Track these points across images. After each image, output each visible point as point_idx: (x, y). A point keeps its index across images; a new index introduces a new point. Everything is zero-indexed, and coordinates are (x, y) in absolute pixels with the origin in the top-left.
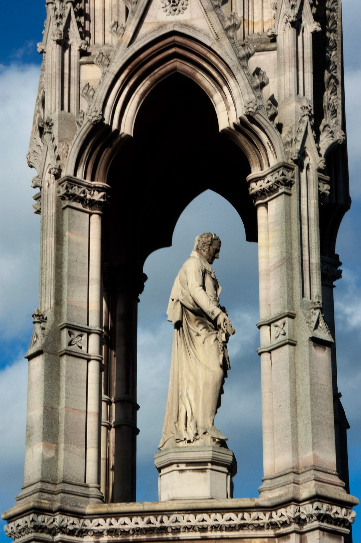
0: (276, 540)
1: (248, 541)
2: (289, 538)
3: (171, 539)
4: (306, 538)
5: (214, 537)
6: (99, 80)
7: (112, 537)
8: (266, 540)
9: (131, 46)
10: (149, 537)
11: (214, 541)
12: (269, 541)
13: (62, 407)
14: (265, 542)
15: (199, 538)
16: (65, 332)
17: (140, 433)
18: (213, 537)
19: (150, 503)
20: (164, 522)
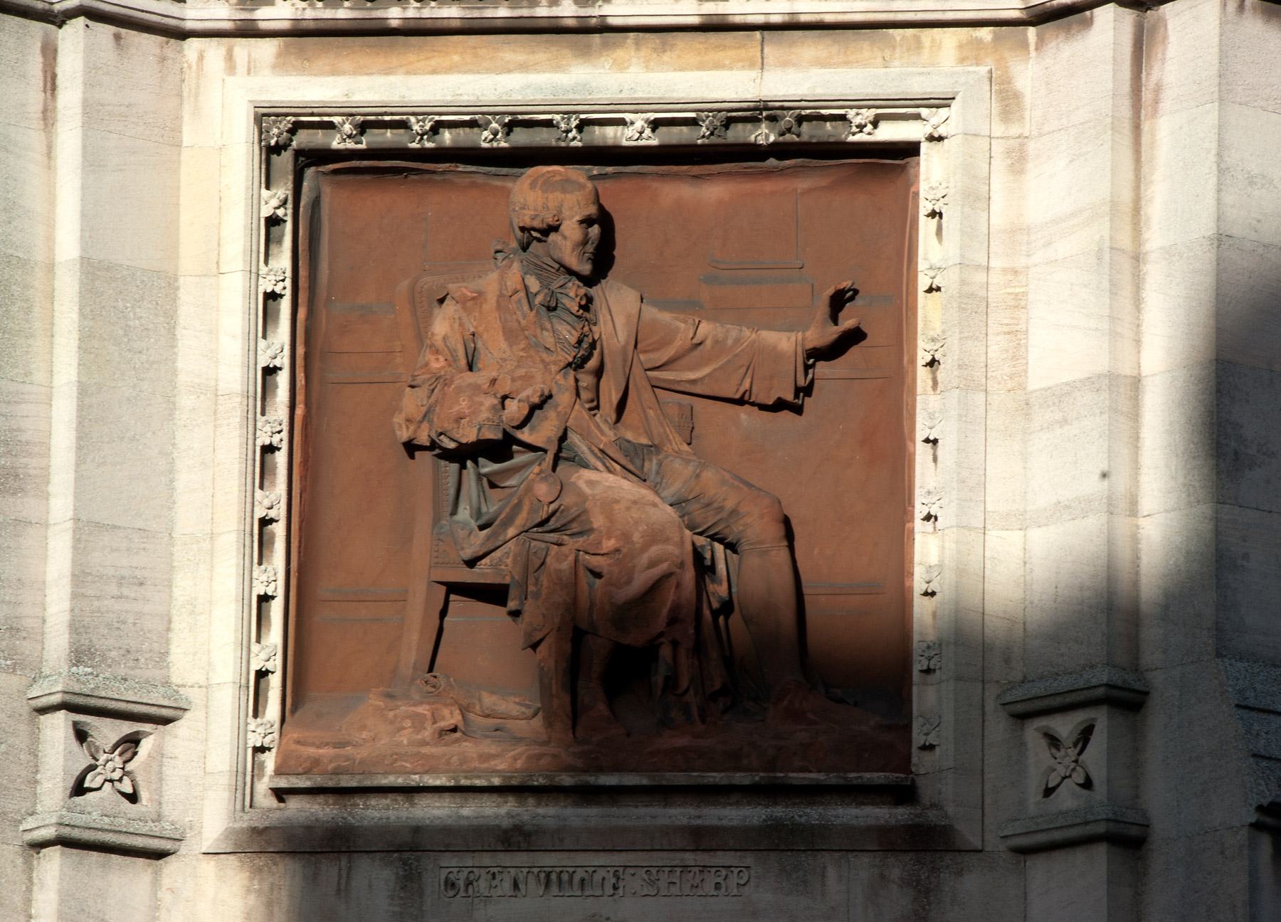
0: (1032, 32)
1: (903, 38)
2: (1089, 23)
3: (571, 23)
4: (1162, 21)
5: (760, 20)
6: (322, 178)
7: (312, 5)
8: (985, 33)
9: (588, 573)
10: (476, 14)
11: (758, 34)
12: (996, 39)
13: (275, 342)
14: (979, 41)
15: (695, 20)
16: (59, 725)
17: (867, 339)
18: (751, 19)
19: (625, 143)
20: (657, 131)
